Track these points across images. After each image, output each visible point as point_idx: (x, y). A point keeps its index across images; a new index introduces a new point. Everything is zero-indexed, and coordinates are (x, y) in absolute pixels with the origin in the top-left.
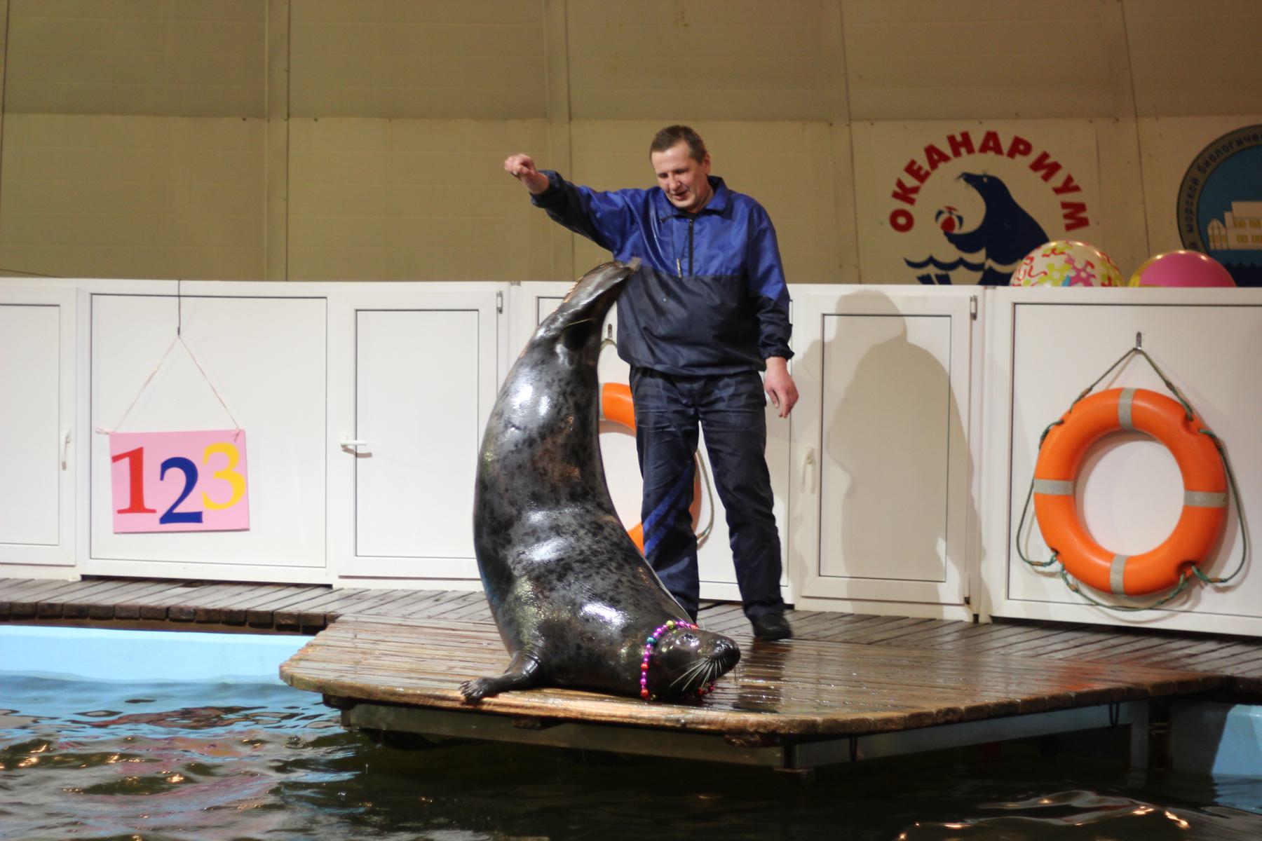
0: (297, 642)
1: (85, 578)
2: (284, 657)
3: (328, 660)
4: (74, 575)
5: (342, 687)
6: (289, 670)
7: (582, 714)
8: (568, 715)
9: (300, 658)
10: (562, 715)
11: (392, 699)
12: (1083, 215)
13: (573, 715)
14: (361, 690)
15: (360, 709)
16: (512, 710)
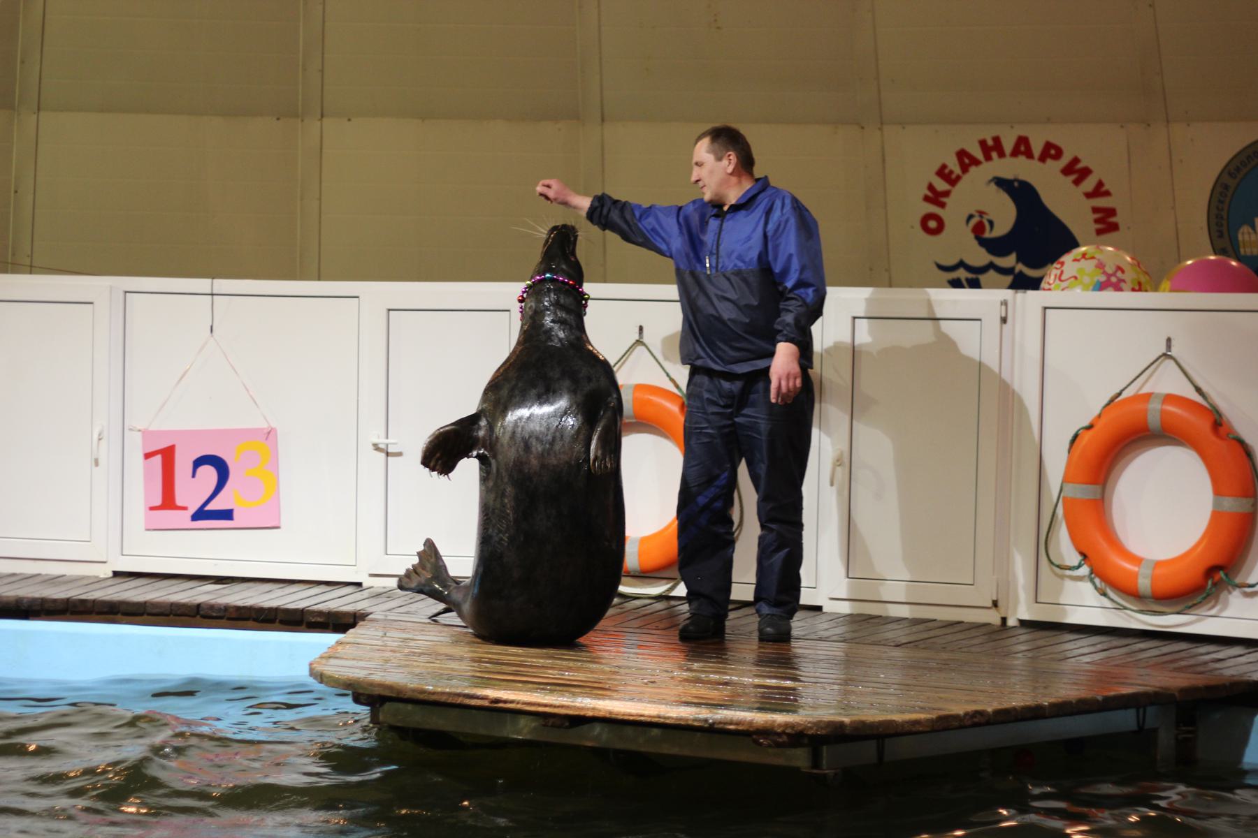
0: (328, 639)
5: (372, 684)
6: (319, 668)
7: (611, 713)
8: (596, 714)
9: (329, 656)
10: (590, 714)
11: (421, 697)
13: (601, 714)
14: (390, 687)
16: (541, 709)
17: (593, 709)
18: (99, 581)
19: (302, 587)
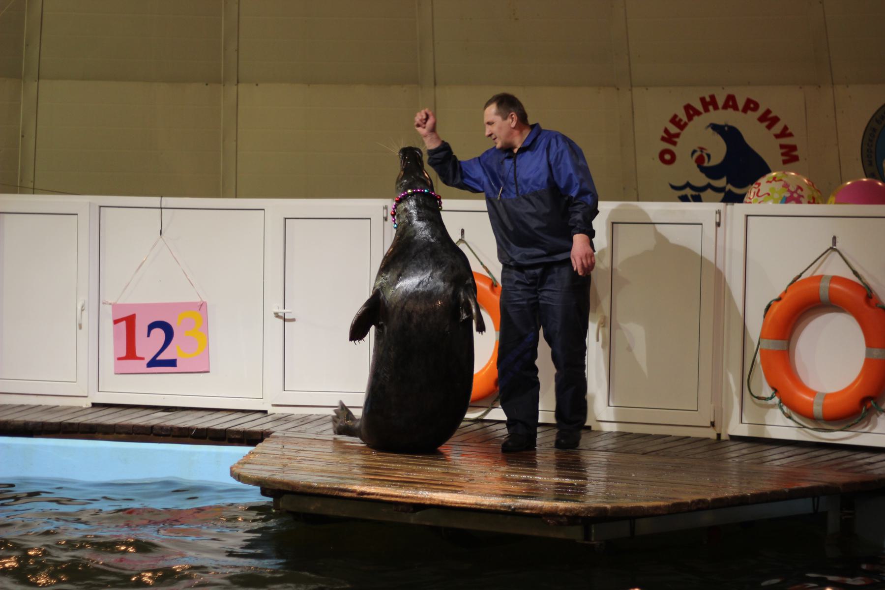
0: (243, 451)
1: (94, 405)
2: (234, 462)
3: (267, 462)
4: (86, 403)
5: (275, 482)
6: (237, 471)
7: (442, 502)
8: (432, 502)
9: (245, 462)
10: (428, 502)
12: (795, 153)
13: (436, 502)
14: (287, 484)
15: (285, 498)
16: (393, 499)
17: (430, 499)
18: (82, 409)
19: (225, 413)
